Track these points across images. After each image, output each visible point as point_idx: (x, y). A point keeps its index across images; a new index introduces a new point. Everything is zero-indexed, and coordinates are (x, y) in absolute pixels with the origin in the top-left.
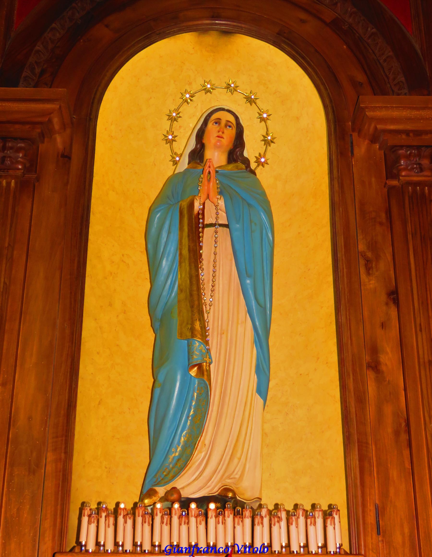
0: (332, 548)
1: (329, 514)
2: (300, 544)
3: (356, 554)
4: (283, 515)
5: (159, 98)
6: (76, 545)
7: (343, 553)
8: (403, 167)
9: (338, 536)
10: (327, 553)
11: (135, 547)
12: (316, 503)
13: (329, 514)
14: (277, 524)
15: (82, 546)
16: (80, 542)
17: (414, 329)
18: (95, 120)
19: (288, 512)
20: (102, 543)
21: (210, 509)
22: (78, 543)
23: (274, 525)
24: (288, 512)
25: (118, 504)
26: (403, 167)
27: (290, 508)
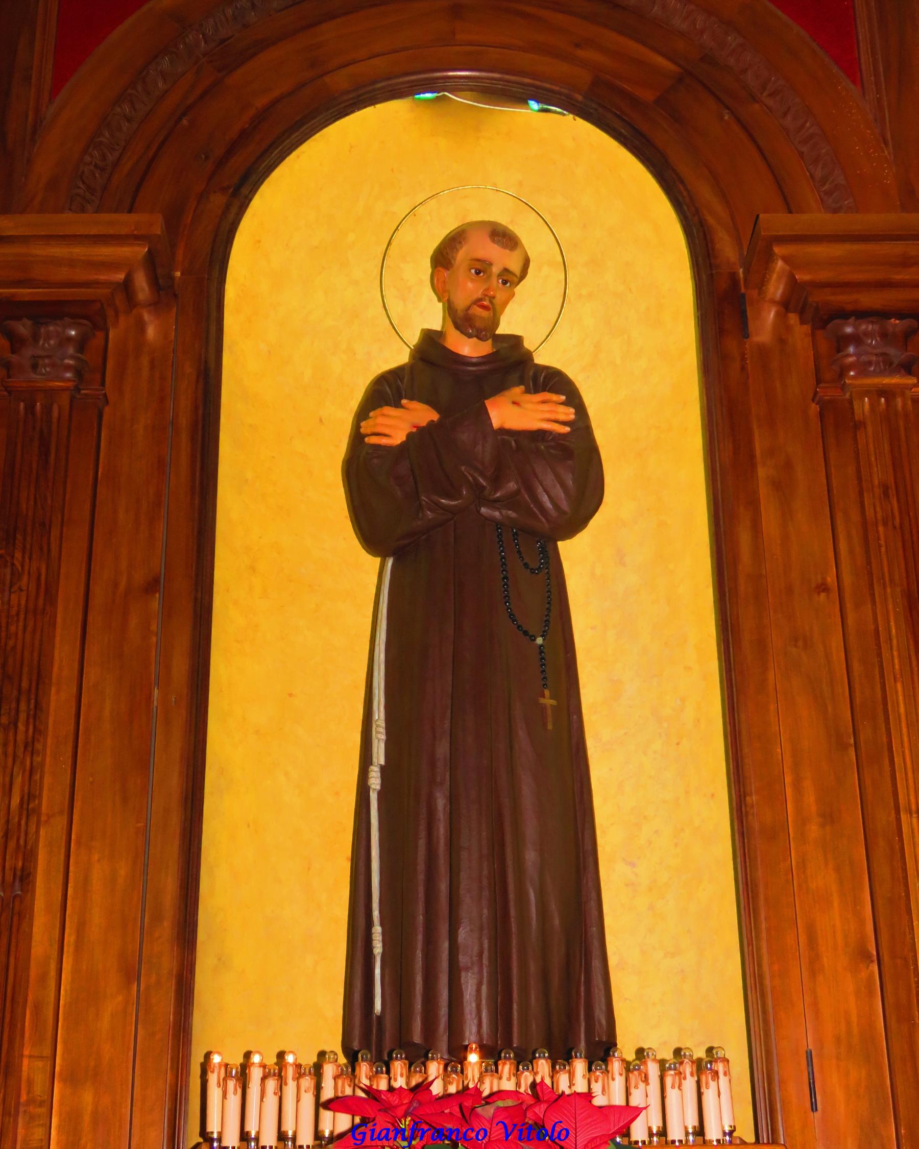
0: (713, 1133)
1: (706, 1066)
2: (723, 1127)
3: (768, 1143)
4: (653, 1070)
5: (337, 260)
6: (201, 1140)
7: (738, 1142)
8: (851, 359)
9: (727, 1107)
10: (705, 1142)
11: (245, 1143)
12: (645, 1047)
13: (706, 1066)
14: (713, 1084)
15: (212, 1140)
16: (248, 1132)
17: (73, 837)
18: (625, 138)
19: (662, 1063)
20: (253, 1135)
21: (470, 1063)
22: (204, 1132)
23: (636, 1087)
24: (662, 1063)
25: (281, 1055)
26: (851, 359)
27: (700, 1053)
